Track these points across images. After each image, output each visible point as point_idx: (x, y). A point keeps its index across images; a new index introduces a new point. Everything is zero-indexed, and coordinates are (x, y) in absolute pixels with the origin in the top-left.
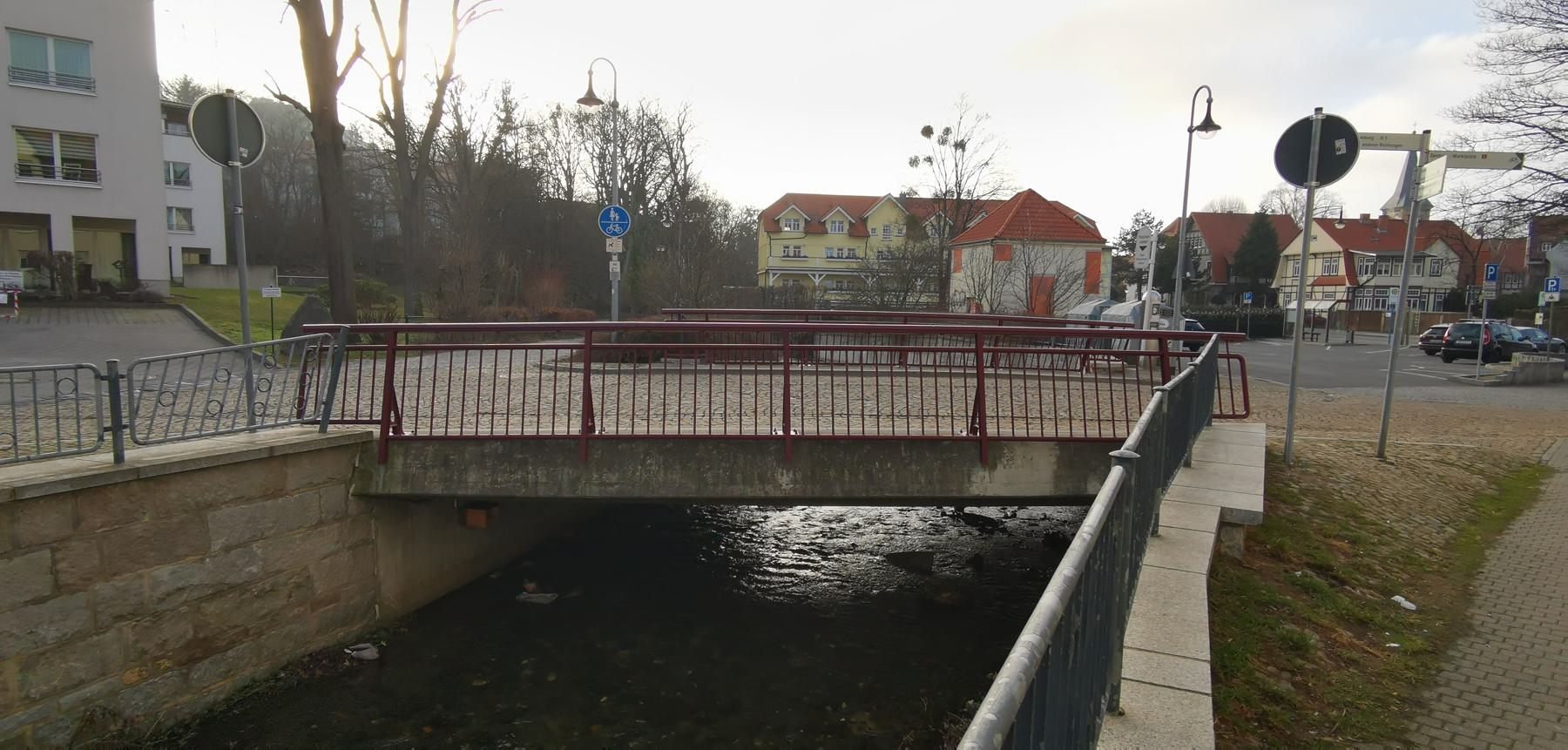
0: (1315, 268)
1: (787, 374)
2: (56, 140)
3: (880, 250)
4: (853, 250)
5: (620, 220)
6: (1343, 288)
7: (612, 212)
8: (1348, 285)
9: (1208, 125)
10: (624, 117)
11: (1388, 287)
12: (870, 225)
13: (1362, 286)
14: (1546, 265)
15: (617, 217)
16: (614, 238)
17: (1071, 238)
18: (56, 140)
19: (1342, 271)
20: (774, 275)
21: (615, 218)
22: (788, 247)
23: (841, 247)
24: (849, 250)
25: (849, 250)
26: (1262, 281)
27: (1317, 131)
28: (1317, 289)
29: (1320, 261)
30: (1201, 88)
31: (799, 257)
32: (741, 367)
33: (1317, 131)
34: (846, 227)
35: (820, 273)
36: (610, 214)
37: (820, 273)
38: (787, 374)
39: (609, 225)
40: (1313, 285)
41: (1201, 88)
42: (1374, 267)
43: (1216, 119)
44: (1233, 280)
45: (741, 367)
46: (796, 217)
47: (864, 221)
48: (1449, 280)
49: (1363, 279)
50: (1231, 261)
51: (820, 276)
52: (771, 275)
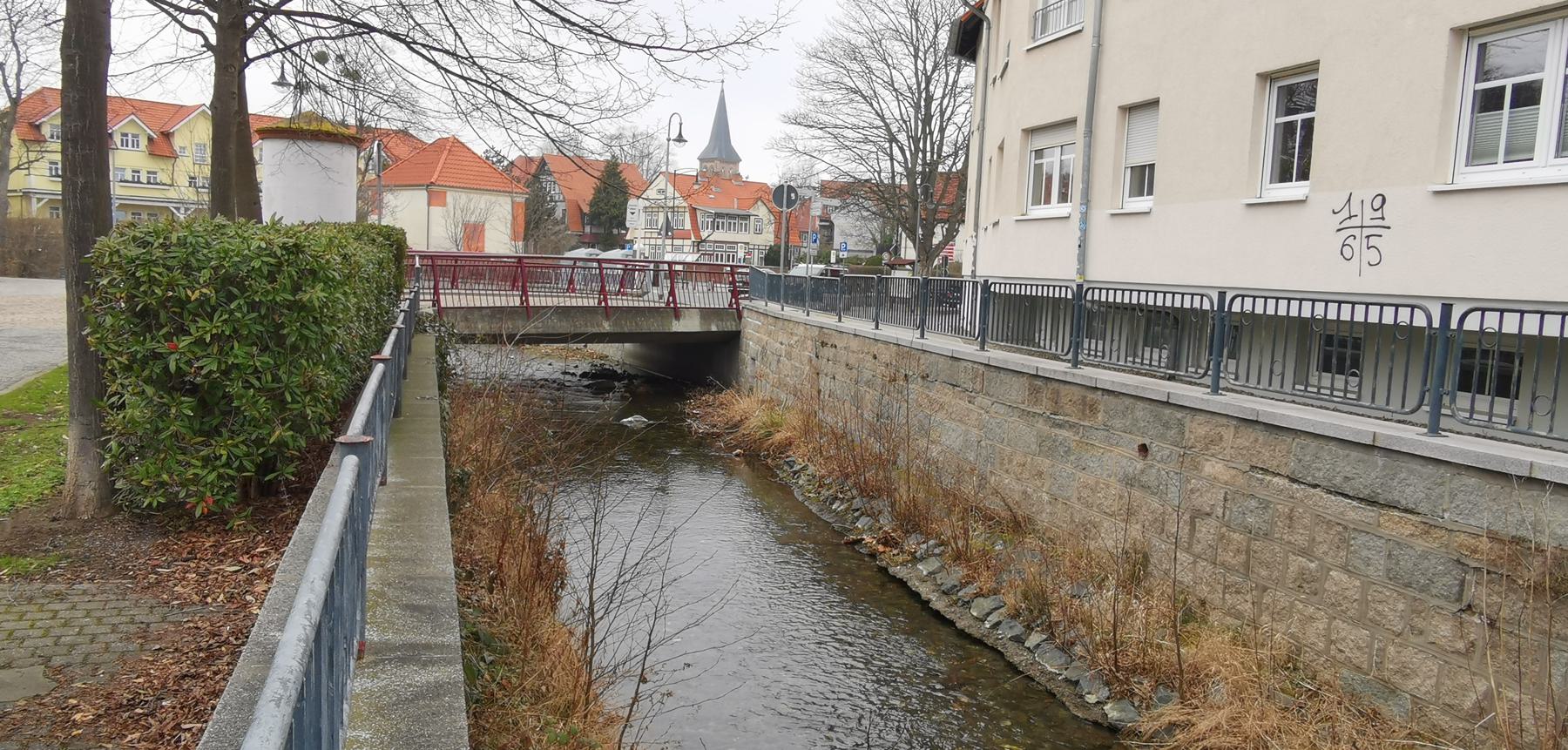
1: (924, 312)
3: (192, 175)
4: (155, 173)
6: (688, 242)
8: (693, 239)
9: (680, 139)
10: (900, 188)
11: (737, 243)
12: (178, 142)
13: (704, 241)
14: (831, 227)
17: (458, 185)
19: (688, 226)
20: (39, 200)
22: (139, 172)
23: (136, 169)
24: (149, 172)
25: (133, 171)
26: (615, 231)
31: (157, 184)
34: (143, 142)
35: (38, 196)
37: (38, 196)
38: (924, 312)
42: (713, 222)
43: (685, 136)
44: (588, 229)
46: (135, 132)
47: (167, 136)
48: (767, 238)
49: (704, 234)
50: (586, 209)
51: (186, 210)
52: (34, 200)
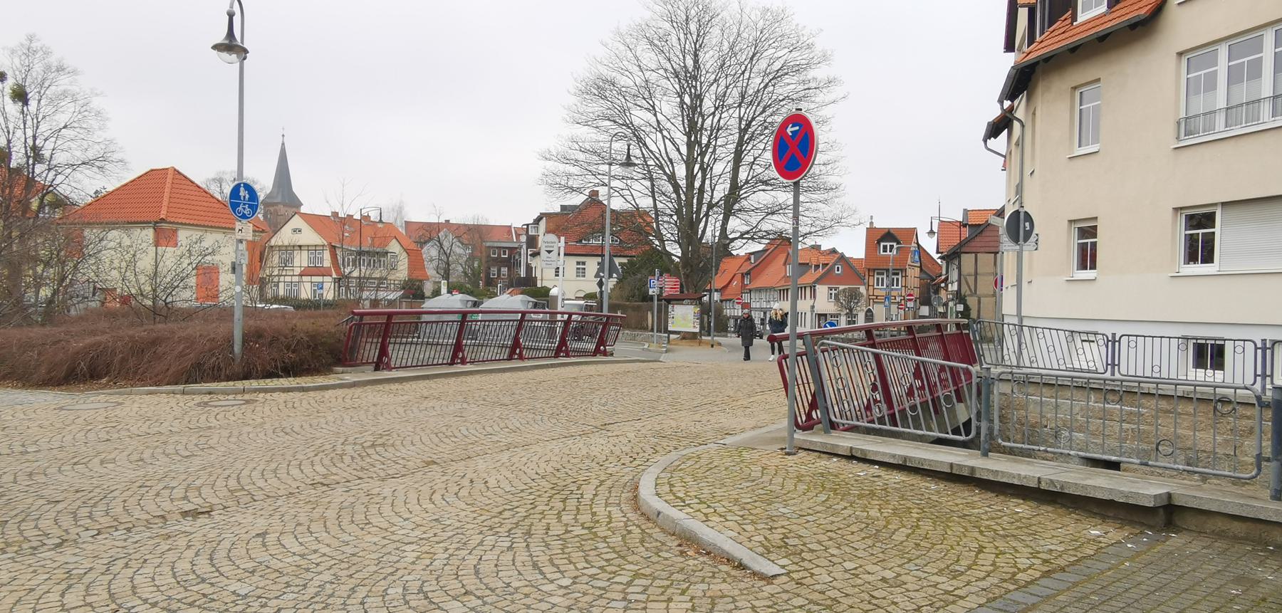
0: (301, 260)
2: (1277, 50)
5: (250, 200)
7: (242, 189)
8: (334, 276)
15: (247, 196)
16: (244, 221)
18: (1277, 50)
19: (327, 263)
21: (244, 197)
27: (170, 177)
28: (305, 278)
29: (305, 254)
30: (989, 149)
32: (1269, 348)
33: (170, 177)
36: (239, 192)
39: (238, 205)
40: (301, 275)
41: (989, 149)
45: (1269, 348)
